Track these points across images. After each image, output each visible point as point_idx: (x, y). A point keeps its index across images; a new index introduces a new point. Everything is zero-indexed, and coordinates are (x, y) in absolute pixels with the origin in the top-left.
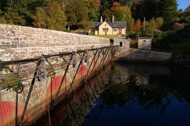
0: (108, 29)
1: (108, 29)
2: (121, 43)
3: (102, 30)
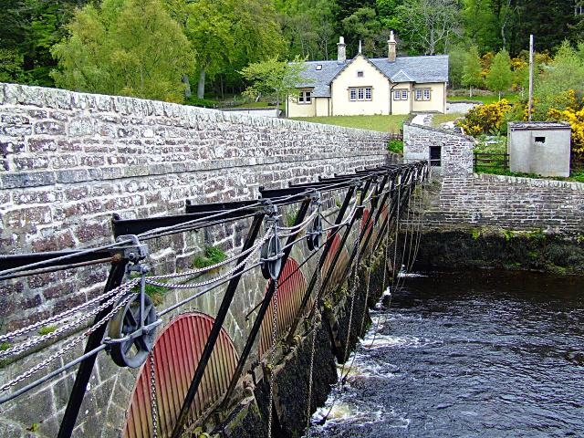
0: (369, 89)
1: (369, 89)
2: (435, 151)
3: (347, 94)
